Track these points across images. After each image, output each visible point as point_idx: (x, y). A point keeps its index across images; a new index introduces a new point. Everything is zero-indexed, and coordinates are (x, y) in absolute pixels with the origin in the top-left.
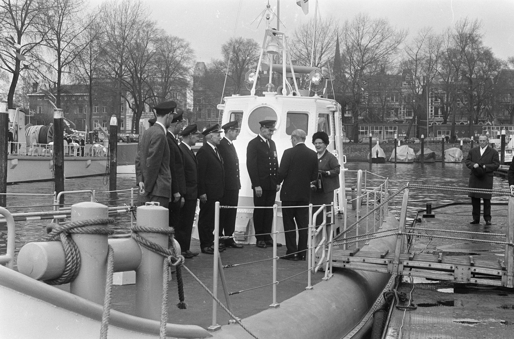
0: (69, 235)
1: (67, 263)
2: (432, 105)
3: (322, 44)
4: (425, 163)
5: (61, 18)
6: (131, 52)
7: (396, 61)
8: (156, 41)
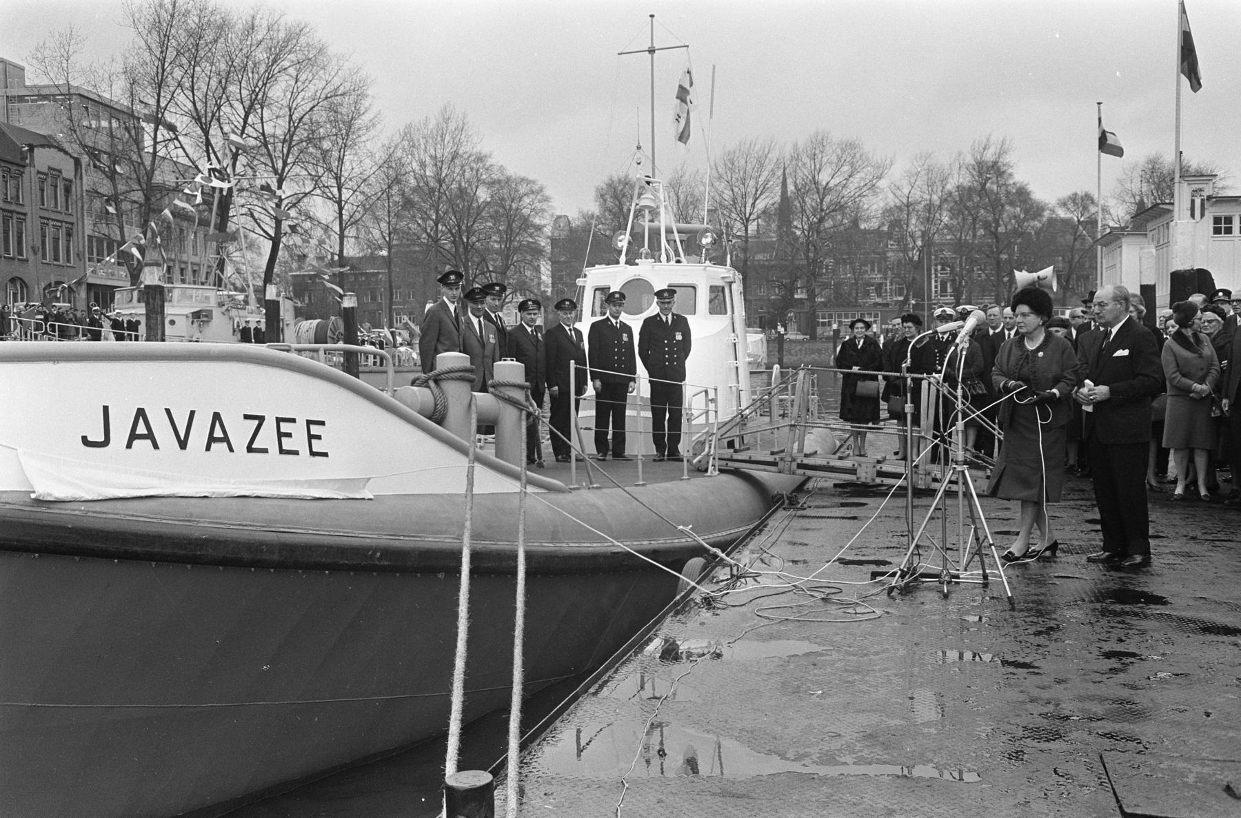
0: (436, 382)
1: (436, 405)
8: (491, 184)
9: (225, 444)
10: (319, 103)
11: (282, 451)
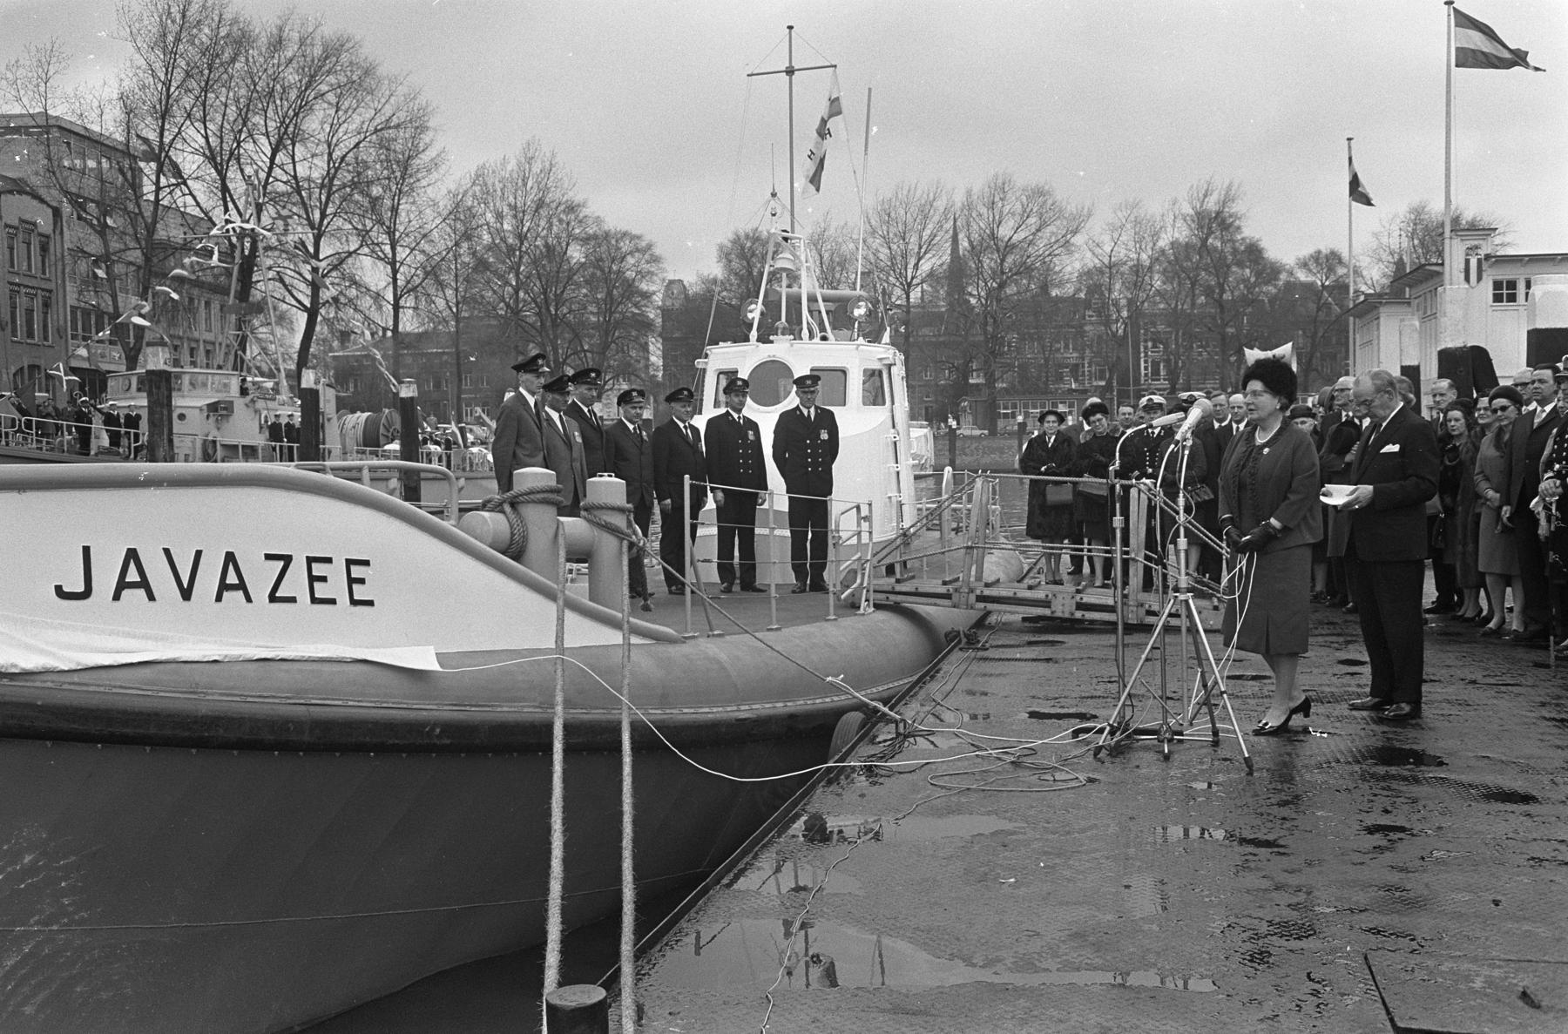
0: (513, 505)
1: (513, 534)
5: (396, 201)
6: (535, 262)
8: (586, 240)
9: (241, 593)
10: (365, 138)
11: (314, 600)
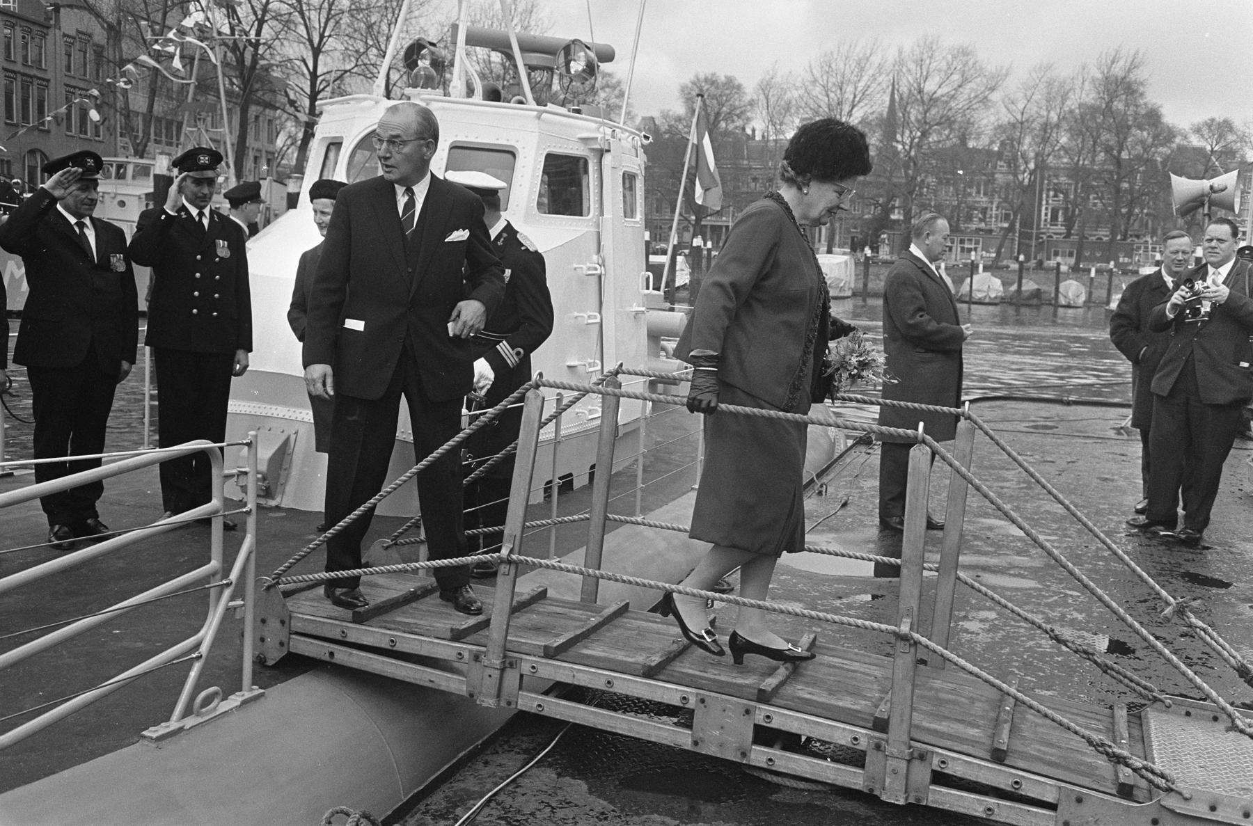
2: (1047, 203)
3: (856, 89)
4: (1023, 305)
7: (985, 122)
